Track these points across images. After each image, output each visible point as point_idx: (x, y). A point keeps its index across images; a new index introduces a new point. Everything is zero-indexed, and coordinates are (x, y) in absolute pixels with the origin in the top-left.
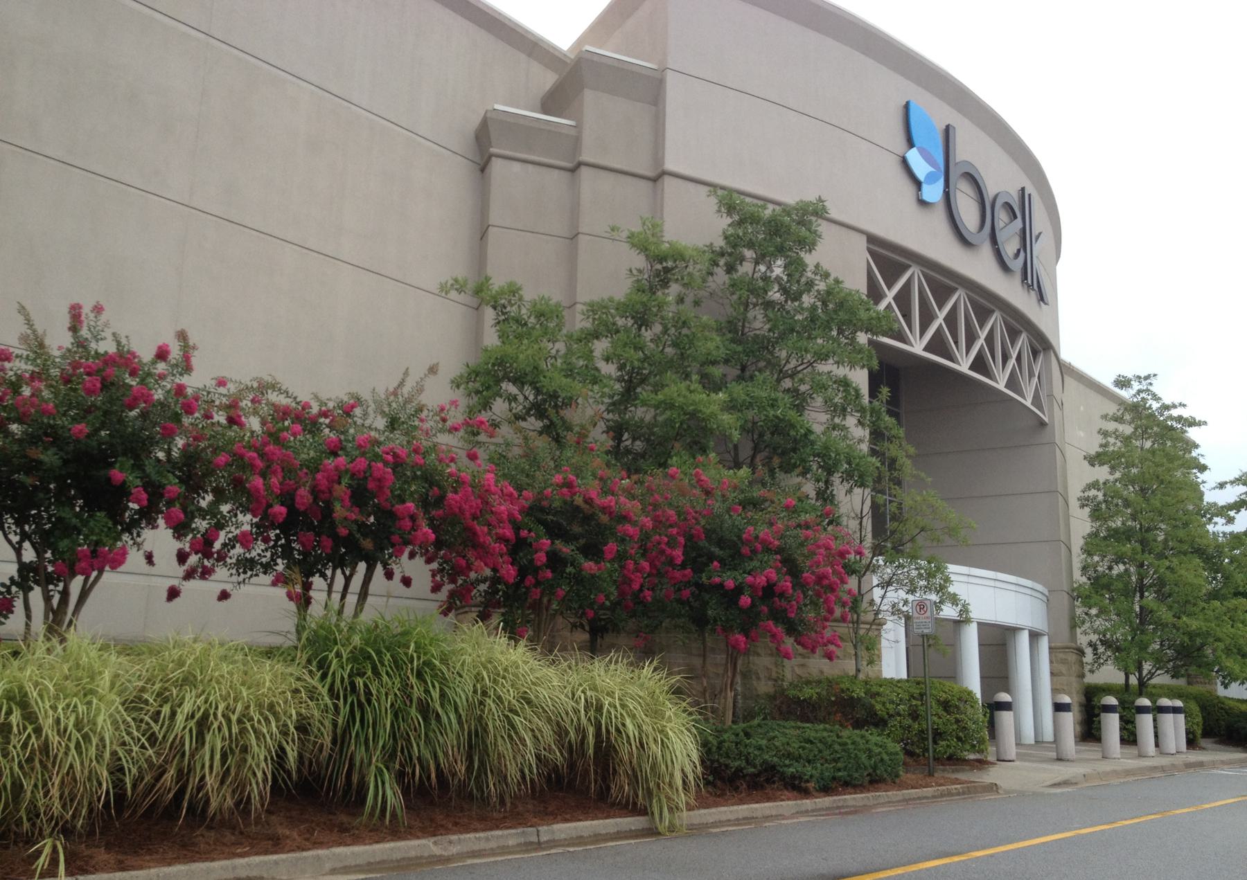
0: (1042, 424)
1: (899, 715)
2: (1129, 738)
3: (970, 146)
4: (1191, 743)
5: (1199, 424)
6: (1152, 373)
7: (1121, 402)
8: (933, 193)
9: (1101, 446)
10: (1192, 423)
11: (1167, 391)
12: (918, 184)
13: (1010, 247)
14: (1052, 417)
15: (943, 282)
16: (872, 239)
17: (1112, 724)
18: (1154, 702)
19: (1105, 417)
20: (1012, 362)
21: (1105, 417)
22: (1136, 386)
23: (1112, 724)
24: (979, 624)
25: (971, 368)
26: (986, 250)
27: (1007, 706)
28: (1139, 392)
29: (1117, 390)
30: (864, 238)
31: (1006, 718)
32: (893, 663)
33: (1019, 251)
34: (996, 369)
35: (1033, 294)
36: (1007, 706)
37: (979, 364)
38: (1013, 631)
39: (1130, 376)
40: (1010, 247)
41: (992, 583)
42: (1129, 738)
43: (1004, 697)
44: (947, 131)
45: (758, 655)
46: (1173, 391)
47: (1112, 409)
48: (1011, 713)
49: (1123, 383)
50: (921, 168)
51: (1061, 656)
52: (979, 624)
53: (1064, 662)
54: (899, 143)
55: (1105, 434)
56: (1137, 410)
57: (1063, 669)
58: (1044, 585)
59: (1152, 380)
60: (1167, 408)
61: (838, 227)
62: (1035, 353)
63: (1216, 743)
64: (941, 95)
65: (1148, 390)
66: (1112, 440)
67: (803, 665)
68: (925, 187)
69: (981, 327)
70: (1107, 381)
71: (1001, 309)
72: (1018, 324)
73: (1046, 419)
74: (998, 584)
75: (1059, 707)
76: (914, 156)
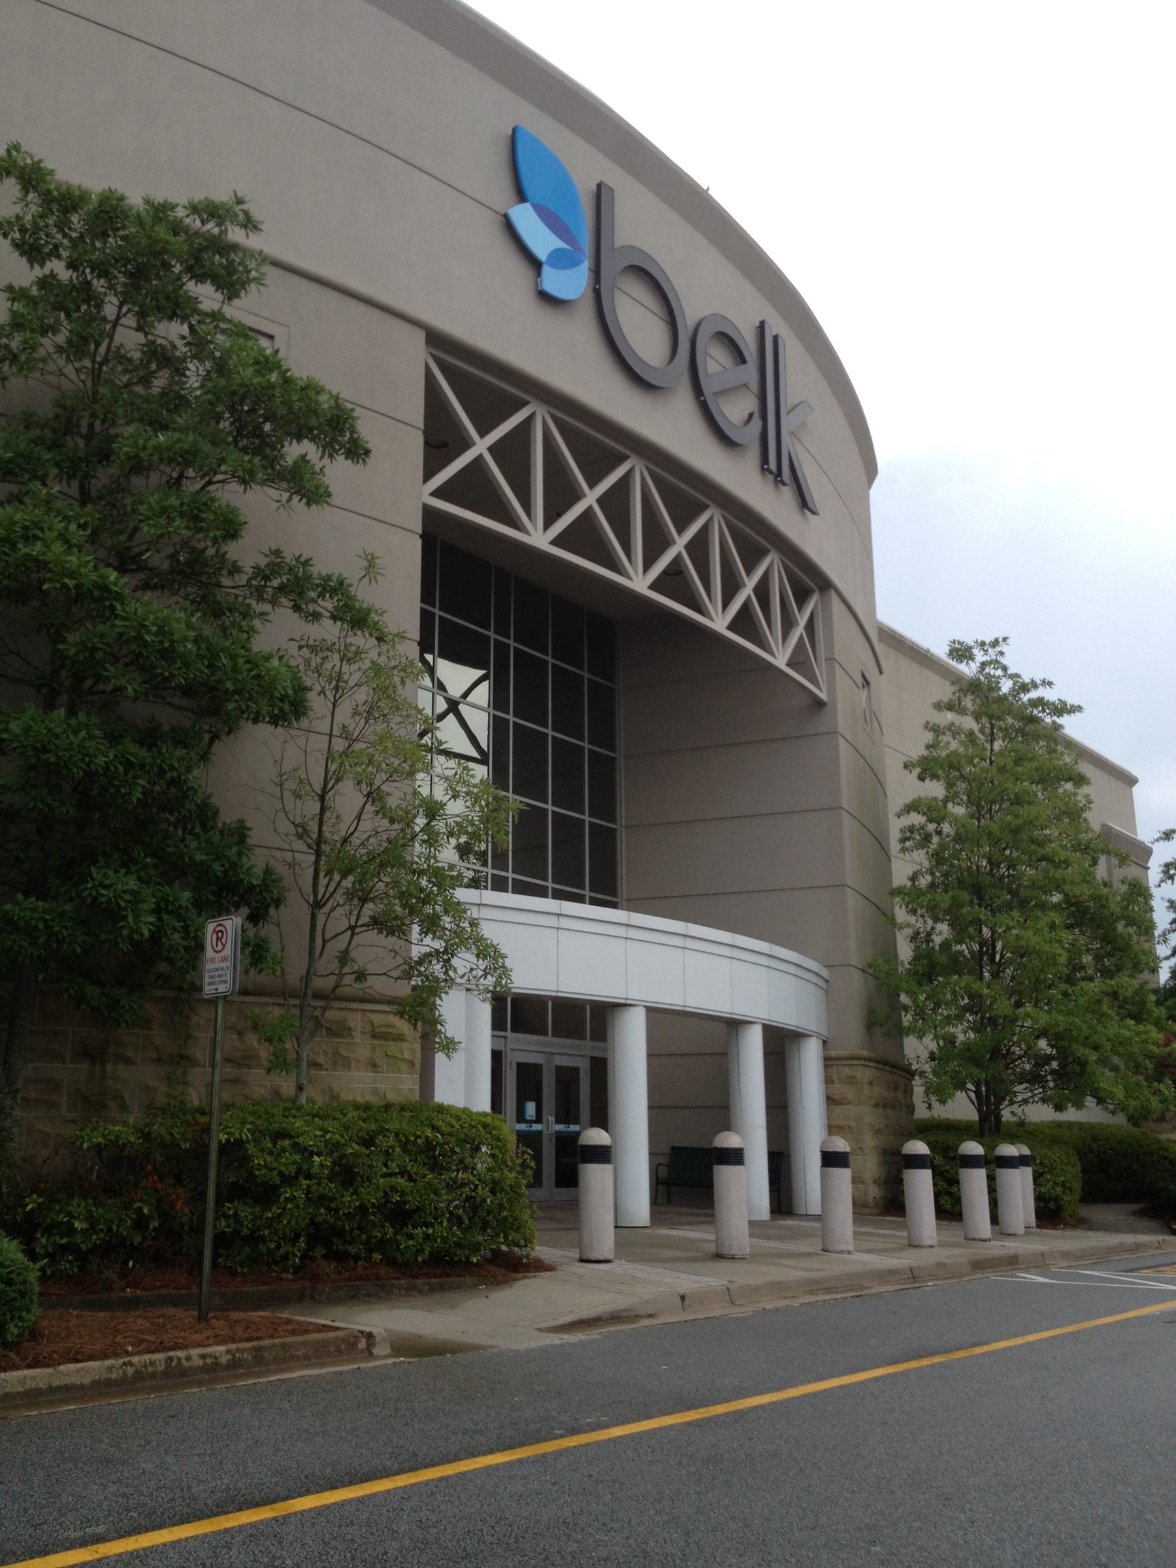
0: (819, 704)
1: (308, 1176)
2: (949, 1208)
3: (640, 224)
4: (1049, 1213)
5: (1076, 709)
6: (1000, 636)
7: (956, 678)
8: (569, 283)
9: (928, 747)
10: (1062, 709)
11: (1023, 661)
12: (536, 264)
13: (736, 411)
14: (832, 690)
15: (598, 442)
16: (436, 340)
17: (921, 1186)
18: (990, 1148)
19: (938, 706)
20: (799, 631)
21: (938, 706)
22: (980, 657)
23: (921, 1186)
24: (649, 1010)
25: (789, 664)
26: (683, 403)
27: (602, 1155)
28: (983, 665)
29: (954, 663)
30: (421, 336)
31: (595, 1176)
32: (463, 1081)
33: (751, 415)
34: (773, 637)
35: (788, 493)
36: (602, 1155)
37: (743, 622)
38: (734, 1025)
39: (970, 641)
40: (736, 411)
41: (727, 951)
42: (949, 1208)
43: (596, 1137)
44: (601, 195)
45: (128, 1061)
46: (1036, 659)
47: (946, 692)
48: (607, 1169)
49: (961, 652)
50: (542, 241)
51: (847, 1071)
52: (649, 1010)
53: (850, 1081)
54: (499, 192)
55: (935, 729)
56: (980, 691)
57: (849, 1092)
58: (818, 961)
59: (1003, 647)
60: (1025, 688)
61: (362, 307)
62: (802, 596)
63: (1140, 1214)
64: (589, 136)
65: (997, 661)
66: (947, 738)
67: (235, 1081)
68: (546, 270)
69: (800, 608)
70: (940, 651)
71: (780, 550)
72: (755, 536)
73: (823, 696)
74: (633, 933)
75: (831, 1160)
76: (525, 218)
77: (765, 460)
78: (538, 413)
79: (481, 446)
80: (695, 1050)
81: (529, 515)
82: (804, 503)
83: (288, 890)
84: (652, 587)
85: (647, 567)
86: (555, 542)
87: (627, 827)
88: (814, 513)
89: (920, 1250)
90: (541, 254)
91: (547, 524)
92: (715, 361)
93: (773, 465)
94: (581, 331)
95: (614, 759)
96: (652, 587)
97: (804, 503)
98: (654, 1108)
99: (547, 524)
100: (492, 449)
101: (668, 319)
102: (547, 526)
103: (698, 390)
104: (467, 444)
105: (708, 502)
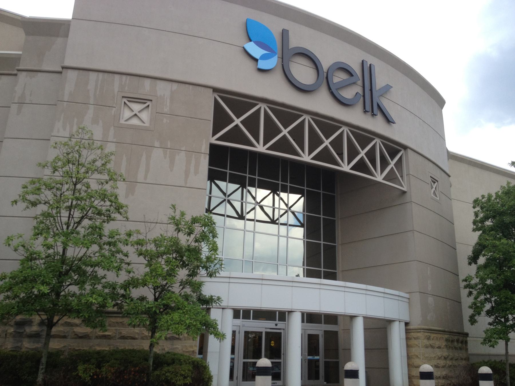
12: (256, 60)
68: (259, 61)
77: (364, 108)
78: (345, 129)
79: (327, 142)
80: (378, 331)
81: (343, 161)
82: (388, 120)
83: (192, 216)
84: (384, 179)
85: (382, 172)
86: (351, 169)
87: (342, 244)
88: (394, 123)
89: (115, 222)
90: (257, 56)
91: (349, 163)
92: (339, 77)
93: (368, 108)
94: (278, 77)
95: (334, 221)
96: (384, 179)
97: (388, 120)
98: (366, 349)
99: (349, 163)
100: (330, 143)
101: (314, 67)
102: (348, 164)
103: (330, 89)
104: (322, 142)
105: (374, 137)
